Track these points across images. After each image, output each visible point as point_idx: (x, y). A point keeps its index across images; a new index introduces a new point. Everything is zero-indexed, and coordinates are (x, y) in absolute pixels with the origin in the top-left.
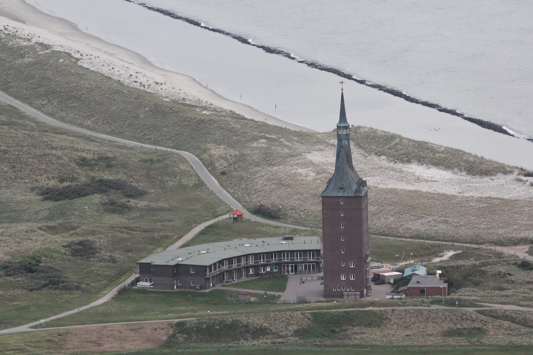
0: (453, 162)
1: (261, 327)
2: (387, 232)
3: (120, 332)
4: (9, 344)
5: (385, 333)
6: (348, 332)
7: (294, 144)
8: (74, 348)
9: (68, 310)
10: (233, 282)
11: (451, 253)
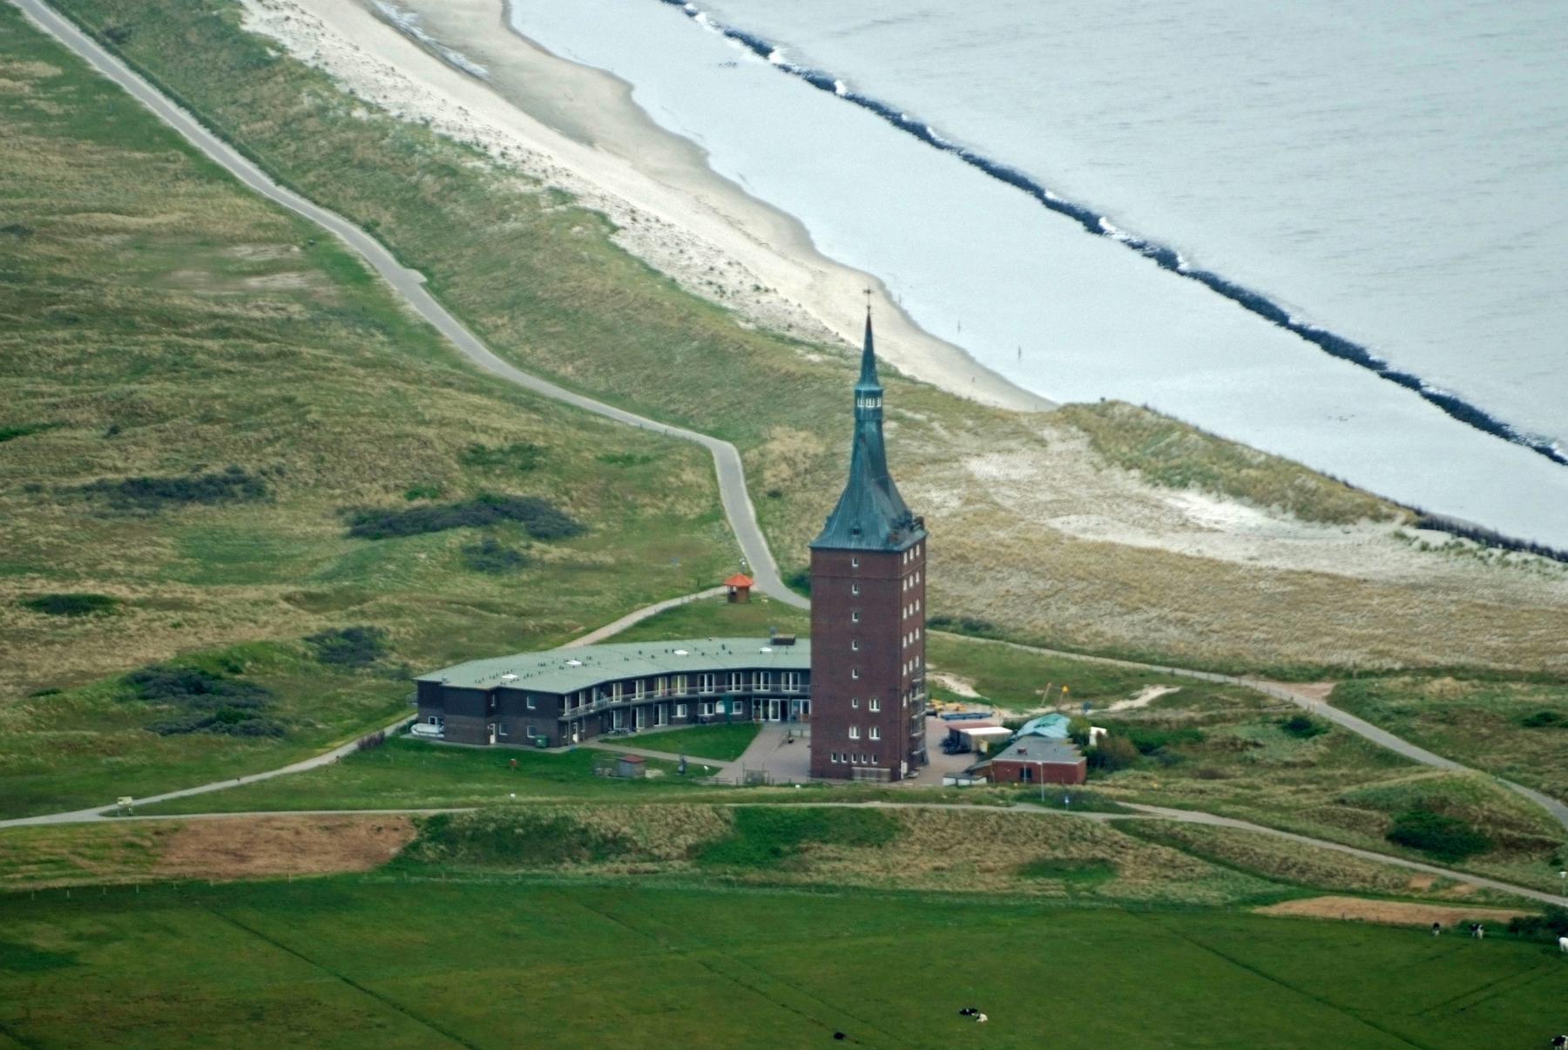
0: (1271, 488)
1: (615, 834)
2: (1048, 640)
3: (298, 833)
4: (33, 848)
5: (889, 861)
6: (807, 856)
7: (956, 435)
8: (181, 864)
9: (221, 779)
10: (631, 735)
11: (1155, 692)
